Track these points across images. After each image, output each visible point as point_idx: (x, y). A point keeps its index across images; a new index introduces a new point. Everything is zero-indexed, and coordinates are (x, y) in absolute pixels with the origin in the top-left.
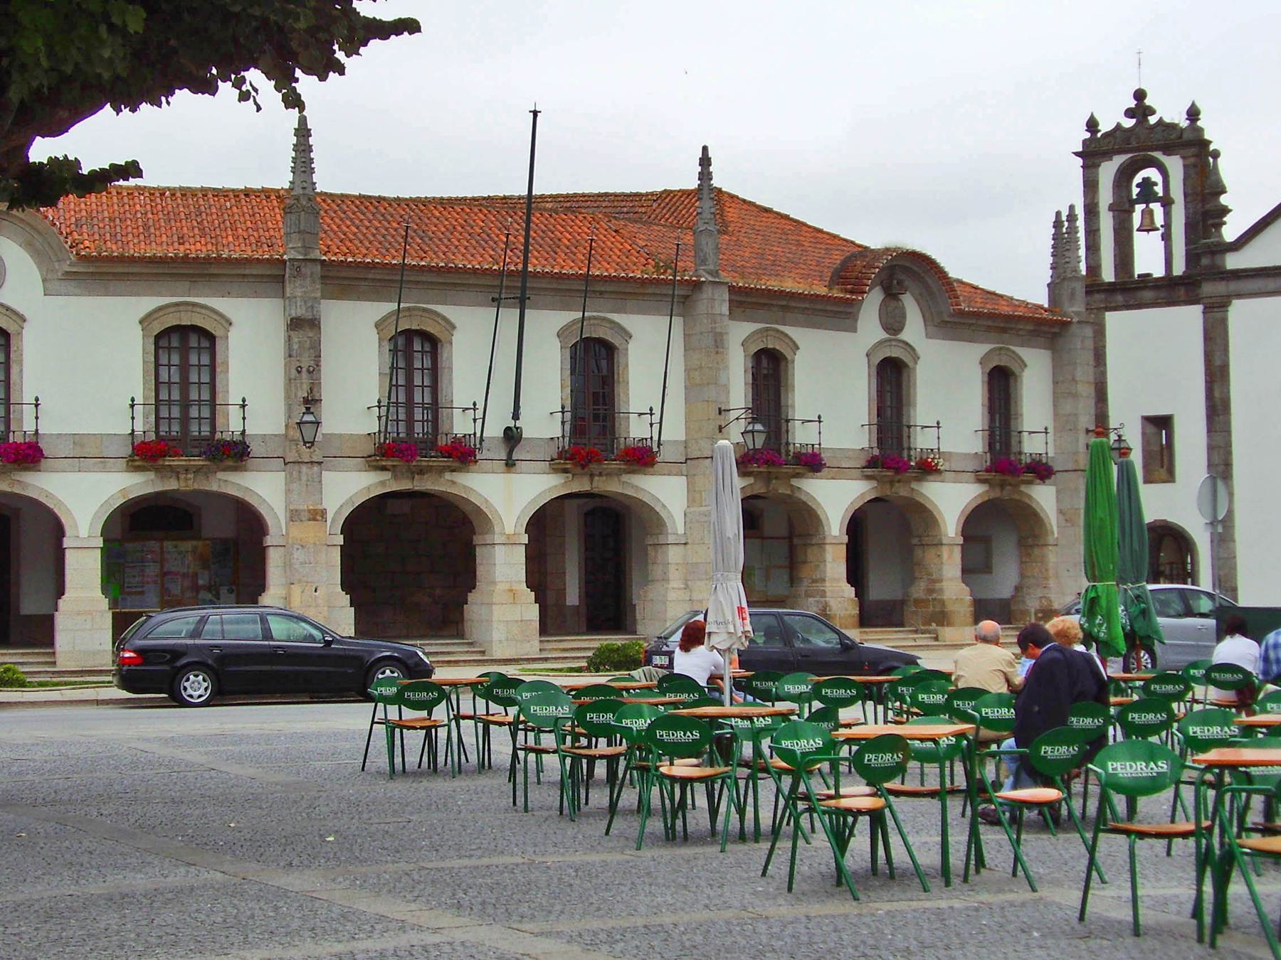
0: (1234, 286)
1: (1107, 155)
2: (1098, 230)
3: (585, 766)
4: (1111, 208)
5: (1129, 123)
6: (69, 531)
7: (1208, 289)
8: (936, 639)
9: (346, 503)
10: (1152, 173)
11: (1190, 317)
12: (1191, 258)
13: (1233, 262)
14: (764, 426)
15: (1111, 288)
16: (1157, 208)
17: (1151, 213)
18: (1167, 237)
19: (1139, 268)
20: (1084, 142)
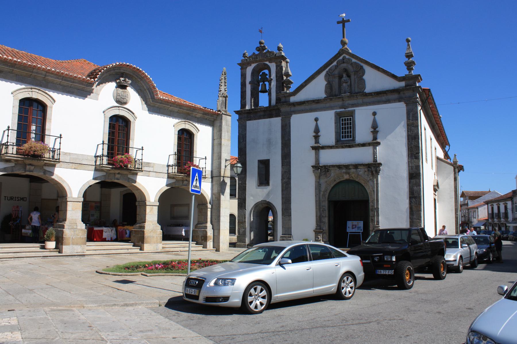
0: (293, 109)
1: (249, 64)
2: (335, 123)
3: (252, 218)
4: (250, 83)
5: (257, 53)
6: (69, 195)
7: (284, 109)
8: (59, 252)
9: (70, 189)
10: (266, 71)
11: (277, 121)
12: (278, 100)
13: (293, 99)
14: (241, 164)
15: (250, 112)
16: (267, 83)
17: (265, 85)
18: (270, 95)
19: (261, 104)
20: (242, 60)
